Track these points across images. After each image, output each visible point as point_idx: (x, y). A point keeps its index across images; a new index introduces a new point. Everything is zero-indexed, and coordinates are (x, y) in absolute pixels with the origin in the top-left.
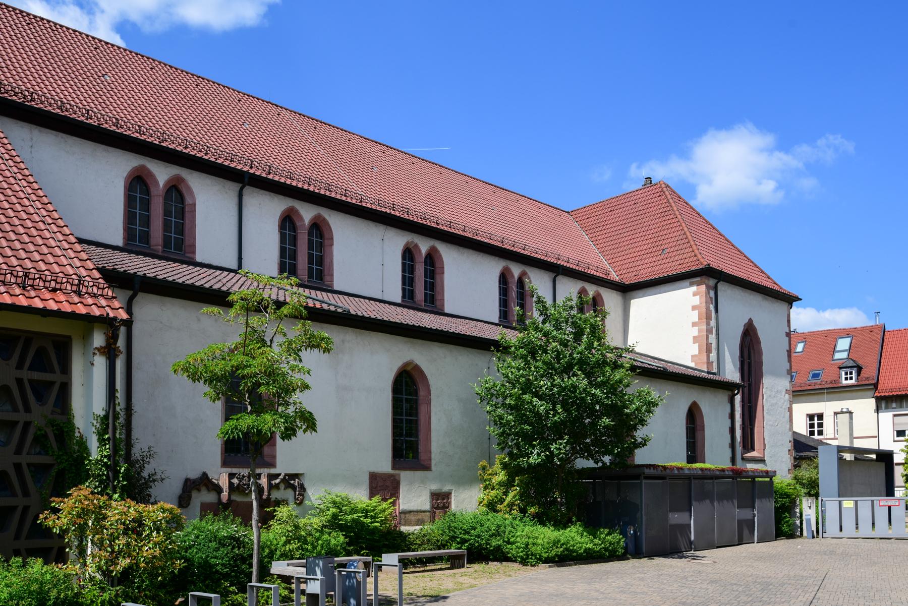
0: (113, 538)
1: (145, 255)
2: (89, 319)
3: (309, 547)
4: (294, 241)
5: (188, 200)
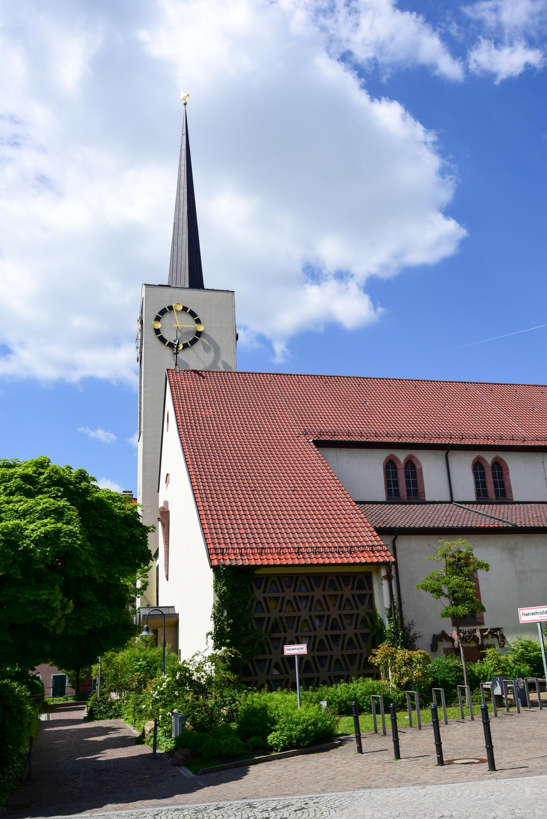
0: (400, 668)
1: (398, 503)
2: (378, 564)
3: (508, 673)
4: (483, 476)
5: (418, 467)
